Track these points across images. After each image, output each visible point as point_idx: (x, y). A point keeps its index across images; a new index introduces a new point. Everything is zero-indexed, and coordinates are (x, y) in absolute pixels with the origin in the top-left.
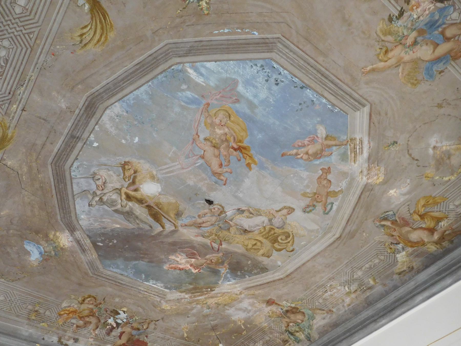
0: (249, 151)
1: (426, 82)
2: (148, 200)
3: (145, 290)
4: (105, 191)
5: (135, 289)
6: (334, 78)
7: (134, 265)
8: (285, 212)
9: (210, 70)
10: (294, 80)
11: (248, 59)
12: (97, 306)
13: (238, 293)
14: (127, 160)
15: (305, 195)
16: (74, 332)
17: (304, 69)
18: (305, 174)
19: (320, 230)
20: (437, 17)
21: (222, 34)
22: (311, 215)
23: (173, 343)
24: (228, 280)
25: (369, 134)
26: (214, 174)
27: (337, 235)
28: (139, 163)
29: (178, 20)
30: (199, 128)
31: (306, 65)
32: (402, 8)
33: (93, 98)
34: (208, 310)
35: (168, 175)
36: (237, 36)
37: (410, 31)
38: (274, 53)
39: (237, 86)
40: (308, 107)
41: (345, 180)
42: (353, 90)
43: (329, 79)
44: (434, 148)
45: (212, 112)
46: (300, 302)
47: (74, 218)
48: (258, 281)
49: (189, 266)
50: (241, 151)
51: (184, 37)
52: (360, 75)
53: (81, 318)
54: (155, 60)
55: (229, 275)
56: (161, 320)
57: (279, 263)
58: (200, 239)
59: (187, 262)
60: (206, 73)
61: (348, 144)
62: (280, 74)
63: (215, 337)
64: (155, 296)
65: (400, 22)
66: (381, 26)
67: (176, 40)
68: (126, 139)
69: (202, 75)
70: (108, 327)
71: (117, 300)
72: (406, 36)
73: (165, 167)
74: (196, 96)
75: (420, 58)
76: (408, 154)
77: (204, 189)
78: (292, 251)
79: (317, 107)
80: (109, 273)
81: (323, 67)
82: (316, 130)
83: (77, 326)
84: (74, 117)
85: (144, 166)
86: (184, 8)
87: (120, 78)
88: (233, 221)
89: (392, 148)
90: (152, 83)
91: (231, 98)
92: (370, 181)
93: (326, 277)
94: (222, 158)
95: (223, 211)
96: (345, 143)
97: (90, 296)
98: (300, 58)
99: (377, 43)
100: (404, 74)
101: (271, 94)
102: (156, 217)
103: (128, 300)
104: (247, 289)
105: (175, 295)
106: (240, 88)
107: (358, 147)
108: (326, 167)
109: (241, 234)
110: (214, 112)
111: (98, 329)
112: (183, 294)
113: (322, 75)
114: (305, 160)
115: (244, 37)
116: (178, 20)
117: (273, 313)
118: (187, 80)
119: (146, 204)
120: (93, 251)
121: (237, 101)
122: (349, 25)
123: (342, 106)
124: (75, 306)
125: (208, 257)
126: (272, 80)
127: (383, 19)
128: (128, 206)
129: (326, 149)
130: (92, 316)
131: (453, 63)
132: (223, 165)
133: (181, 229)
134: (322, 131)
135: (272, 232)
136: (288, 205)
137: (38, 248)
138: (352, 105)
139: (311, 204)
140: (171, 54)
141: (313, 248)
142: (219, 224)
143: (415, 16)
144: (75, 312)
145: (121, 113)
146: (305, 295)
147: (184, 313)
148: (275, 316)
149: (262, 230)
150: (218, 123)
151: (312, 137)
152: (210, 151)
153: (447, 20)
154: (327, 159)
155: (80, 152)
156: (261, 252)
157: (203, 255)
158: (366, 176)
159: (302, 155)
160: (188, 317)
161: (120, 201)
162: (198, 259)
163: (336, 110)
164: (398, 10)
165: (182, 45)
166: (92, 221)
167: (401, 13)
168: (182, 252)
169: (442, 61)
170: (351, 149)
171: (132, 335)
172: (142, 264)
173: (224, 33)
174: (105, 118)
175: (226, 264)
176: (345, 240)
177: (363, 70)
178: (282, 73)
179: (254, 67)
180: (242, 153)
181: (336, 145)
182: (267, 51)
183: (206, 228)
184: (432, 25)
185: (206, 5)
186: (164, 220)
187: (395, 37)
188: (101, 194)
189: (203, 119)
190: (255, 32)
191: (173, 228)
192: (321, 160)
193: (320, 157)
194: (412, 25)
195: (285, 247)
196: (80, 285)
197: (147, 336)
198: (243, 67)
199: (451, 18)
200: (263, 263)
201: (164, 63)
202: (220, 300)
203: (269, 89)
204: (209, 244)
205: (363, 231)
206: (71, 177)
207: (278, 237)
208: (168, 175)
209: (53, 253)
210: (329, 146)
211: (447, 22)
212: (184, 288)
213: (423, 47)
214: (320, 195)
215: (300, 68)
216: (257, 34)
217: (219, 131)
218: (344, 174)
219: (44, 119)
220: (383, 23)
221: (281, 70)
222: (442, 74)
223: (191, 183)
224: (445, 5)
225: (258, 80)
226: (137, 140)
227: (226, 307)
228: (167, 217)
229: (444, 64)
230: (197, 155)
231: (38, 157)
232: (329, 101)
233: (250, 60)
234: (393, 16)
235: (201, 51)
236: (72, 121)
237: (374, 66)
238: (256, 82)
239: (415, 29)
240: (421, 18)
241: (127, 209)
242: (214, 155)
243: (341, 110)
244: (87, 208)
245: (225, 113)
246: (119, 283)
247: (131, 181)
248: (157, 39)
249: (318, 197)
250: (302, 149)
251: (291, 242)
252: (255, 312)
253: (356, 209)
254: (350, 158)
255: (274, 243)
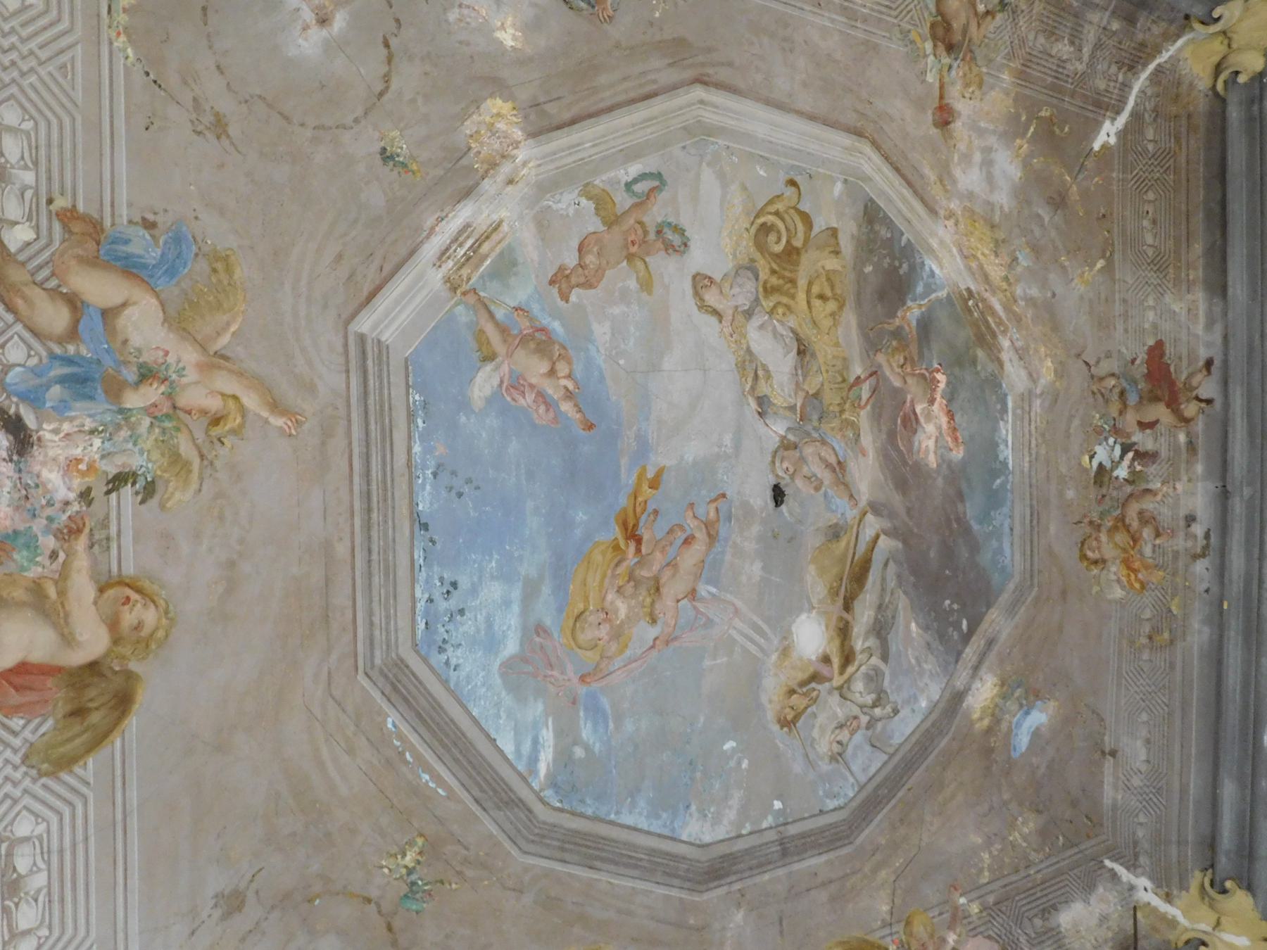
0: (625, 510)
1: (199, 240)
2: (835, 618)
3: (1026, 453)
4: (856, 710)
5: (1033, 473)
6: (356, 479)
7: (980, 523)
8: (711, 298)
9: (516, 734)
10: (421, 561)
11: (448, 689)
12: (1099, 526)
13: (950, 223)
14: (776, 728)
15: (646, 285)
16: (1173, 534)
17: (386, 560)
18: (601, 331)
19: (709, 157)
20: (56, 390)
21: (438, 778)
22: (684, 221)
23: (1131, 282)
24: (930, 280)
25: (412, 253)
26: (712, 538)
27: (699, 92)
28: (770, 702)
29: (470, 873)
30: (639, 652)
31: (375, 565)
32: (108, 492)
33: (699, 883)
34: (1020, 258)
35: (765, 627)
36: (421, 749)
37: (133, 419)
38: (401, 650)
39: (512, 657)
40: (454, 473)
41: (554, 207)
42: (349, 406)
43: (365, 487)
44: (323, 21)
45: (591, 657)
46: (913, 36)
47: (934, 716)
48: (904, 200)
49: (936, 407)
50: (636, 526)
51: (491, 836)
52: (306, 426)
53: (1135, 539)
54: (567, 846)
55: (920, 289)
56: (1084, 357)
57: (838, 188)
58: (867, 440)
59: (929, 417)
60: (525, 738)
61: (468, 287)
62: (430, 600)
63: (1081, 177)
64: (1033, 418)
65: (136, 462)
66: (179, 496)
67: (507, 845)
68: (739, 763)
69: (535, 742)
70: (1139, 468)
71: (1070, 494)
72: (149, 415)
73: (752, 648)
74: (582, 714)
75: (165, 320)
76: (387, 88)
77: (756, 529)
78: (792, 183)
79: (441, 450)
80: (1017, 557)
81: (353, 525)
82: (489, 401)
83: (1158, 535)
84: (749, 882)
85: (772, 687)
86: (442, 882)
87: (636, 873)
88: (792, 401)
89: (402, 148)
90: (609, 813)
91: (542, 647)
92: (518, 134)
93: (818, 20)
94: (671, 551)
95: (786, 446)
96: (471, 299)
97: (1083, 557)
98: (370, 591)
99: (218, 463)
100: (225, 318)
101: (480, 578)
102: (860, 574)
103: (1064, 470)
104: (933, 211)
105: (1015, 376)
106: (511, 647)
107: (461, 252)
108: (555, 291)
109: (813, 355)
110: (589, 654)
111: (1151, 486)
112: (1005, 356)
113: (369, 510)
114: (569, 363)
115: (413, 738)
116: (470, 873)
117: (967, 85)
118: (564, 758)
119: (845, 615)
120: (984, 625)
121: (540, 629)
122: (231, 564)
123: (398, 392)
124: (1115, 569)
125: (897, 383)
126: (453, 603)
127: (162, 507)
128: (867, 644)
129: (516, 332)
130: (1123, 520)
131: (107, 222)
132: (684, 536)
133: (864, 500)
134: (484, 383)
135: (774, 281)
136: (693, 302)
137: (1019, 725)
138: (380, 370)
139: (659, 245)
140: (537, 831)
141: (761, 131)
142: (815, 429)
143: (97, 442)
144: (1127, 563)
145: (696, 815)
146: (890, 39)
147: (1048, 312)
148: (975, 70)
149: (780, 310)
150: (608, 626)
151: (510, 395)
152: (674, 588)
153: (41, 360)
154: (536, 309)
155: (804, 819)
156: (832, 264)
157: (898, 395)
158: (514, 158)
159: (564, 382)
160: (1054, 295)
161: (863, 668)
162: (912, 401)
163: (417, 397)
164: (119, 498)
165: (507, 826)
166: (926, 679)
167: (118, 481)
168: (910, 450)
169: (128, 257)
170: (477, 267)
171: (1141, 398)
172: (971, 510)
173: (431, 777)
174: (722, 832)
175: (897, 322)
176: (701, 59)
177: (293, 432)
178: (427, 596)
179: (453, 661)
180: (637, 520)
181: (491, 316)
182: (407, 671)
183: (837, 448)
184: (80, 382)
185: (408, 853)
186: (862, 548)
187: (172, 437)
188: (865, 714)
189: (618, 662)
190: (390, 726)
191: (870, 517)
192: (545, 321)
193: (542, 330)
194: (118, 427)
195: (792, 211)
196: (1064, 593)
197: (1133, 361)
198: (468, 683)
199: (29, 356)
200: (855, 230)
201: (561, 827)
202: (984, 251)
203: (474, 591)
204: (869, 407)
205: (651, 24)
206: (859, 791)
207: (778, 252)
208: (765, 627)
209: (1018, 692)
210: (503, 330)
211: (44, 354)
212: (991, 367)
213: (137, 345)
214: (626, 239)
215: (389, 572)
216: (390, 720)
217: (622, 608)
218: (543, 223)
219: (781, 924)
220: (169, 499)
221: (420, 606)
222: (151, 217)
223: (756, 569)
224: (17, 405)
225: (472, 631)
226: (729, 745)
227: (997, 219)
228: (851, 551)
229: (127, 242)
230: (695, 608)
231: (854, 873)
232: (410, 437)
233: (445, 683)
234: (137, 493)
235: (494, 784)
236: (757, 879)
237: (265, 414)
238: (478, 631)
239: (121, 411)
240: (89, 424)
241: (872, 642)
242: (674, 575)
243: (408, 386)
244: (904, 712)
245: (578, 633)
246: (1031, 521)
247: (813, 685)
248: (527, 878)
249: (633, 243)
250: (550, 391)
251: (772, 209)
252: (981, 133)
253: (608, 103)
254: (498, 250)
255: (798, 251)
